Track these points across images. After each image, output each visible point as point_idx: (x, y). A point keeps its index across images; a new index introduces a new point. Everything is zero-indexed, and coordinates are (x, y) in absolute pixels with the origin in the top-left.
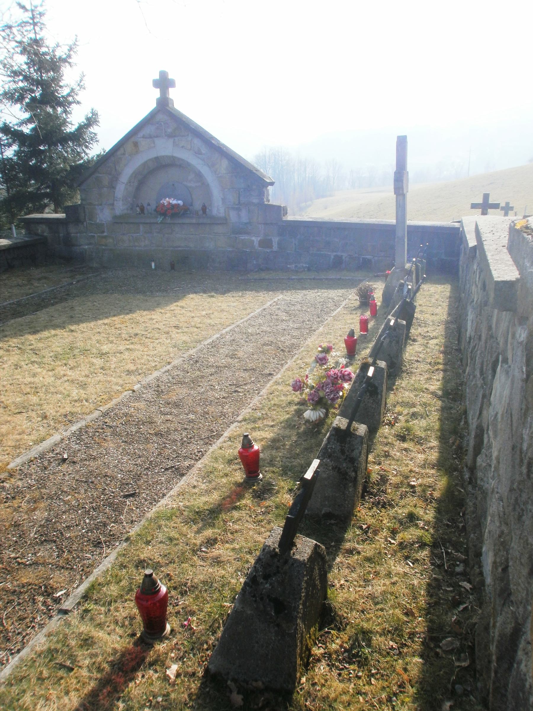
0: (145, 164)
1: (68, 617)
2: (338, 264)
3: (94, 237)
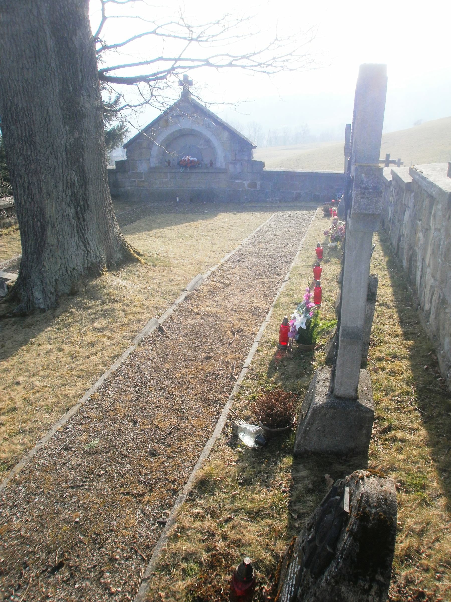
0: (172, 134)
2: (297, 198)
3: (135, 181)
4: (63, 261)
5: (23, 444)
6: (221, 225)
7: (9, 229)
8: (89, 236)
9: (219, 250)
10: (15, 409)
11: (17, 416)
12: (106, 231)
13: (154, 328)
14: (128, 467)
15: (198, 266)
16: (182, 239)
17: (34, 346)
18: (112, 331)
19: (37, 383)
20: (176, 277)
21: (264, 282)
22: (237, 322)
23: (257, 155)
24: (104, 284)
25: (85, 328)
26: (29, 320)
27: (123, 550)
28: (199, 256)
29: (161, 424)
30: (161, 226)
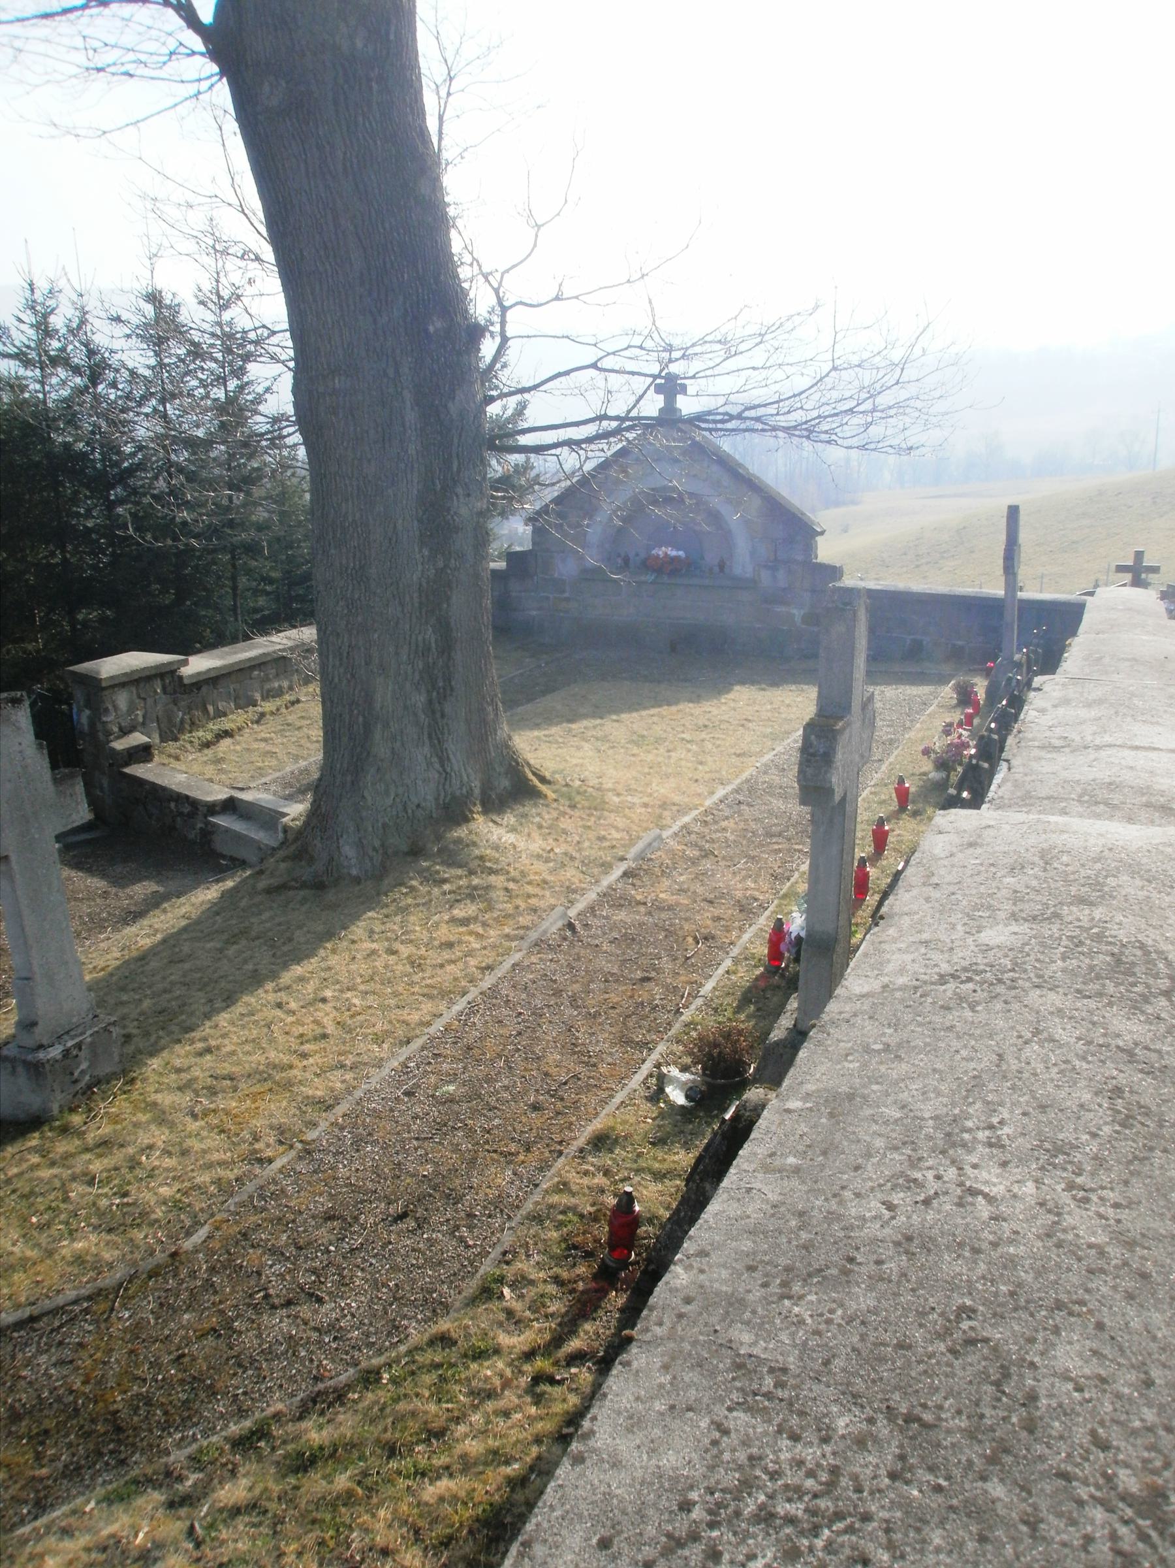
3: (547, 598)
4: (401, 790)
5: (343, 1082)
6: (725, 717)
7: (278, 702)
8: (451, 746)
9: (707, 776)
10: (324, 1036)
11: (331, 1045)
12: (482, 732)
13: (560, 924)
14: (496, 1122)
15: (658, 811)
16: (638, 746)
17: (345, 943)
18: (485, 924)
19: (356, 1001)
20: (613, 832)
21: (780, 850)
22: (709, 922)
23: (826, 551)
24: (475, 839)
25: (436, 918)
26: (330, 896)
27: (485, 1207)
28: (663, 789)
29: (553, 1071)
30: (599, 712)
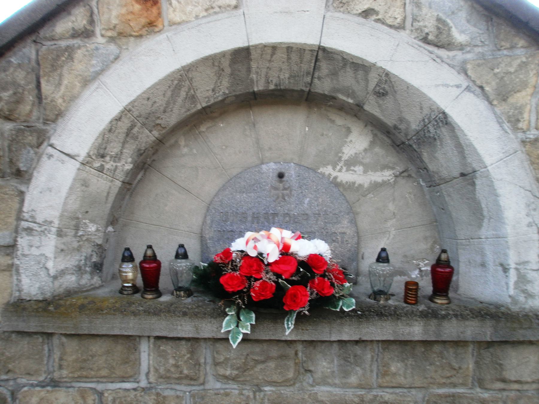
0: (183, 78)
1: (17, 289)
